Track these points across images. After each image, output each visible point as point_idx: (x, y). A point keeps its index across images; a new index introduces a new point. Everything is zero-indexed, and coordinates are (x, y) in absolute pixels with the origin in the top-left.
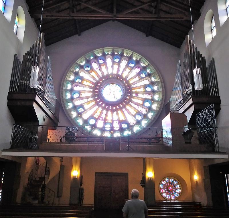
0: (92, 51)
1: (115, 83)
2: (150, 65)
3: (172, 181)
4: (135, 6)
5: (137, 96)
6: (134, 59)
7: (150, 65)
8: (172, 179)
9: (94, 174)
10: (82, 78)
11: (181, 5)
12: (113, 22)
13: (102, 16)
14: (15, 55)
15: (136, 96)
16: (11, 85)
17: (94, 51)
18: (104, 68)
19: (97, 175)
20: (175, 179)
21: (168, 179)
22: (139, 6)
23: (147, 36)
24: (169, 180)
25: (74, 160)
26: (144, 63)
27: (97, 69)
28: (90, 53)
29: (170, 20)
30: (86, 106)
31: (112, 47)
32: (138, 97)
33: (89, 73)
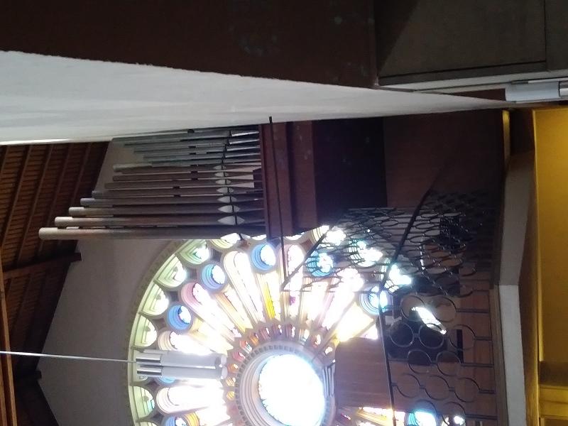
2: (179, 253)
26: (175, 269)
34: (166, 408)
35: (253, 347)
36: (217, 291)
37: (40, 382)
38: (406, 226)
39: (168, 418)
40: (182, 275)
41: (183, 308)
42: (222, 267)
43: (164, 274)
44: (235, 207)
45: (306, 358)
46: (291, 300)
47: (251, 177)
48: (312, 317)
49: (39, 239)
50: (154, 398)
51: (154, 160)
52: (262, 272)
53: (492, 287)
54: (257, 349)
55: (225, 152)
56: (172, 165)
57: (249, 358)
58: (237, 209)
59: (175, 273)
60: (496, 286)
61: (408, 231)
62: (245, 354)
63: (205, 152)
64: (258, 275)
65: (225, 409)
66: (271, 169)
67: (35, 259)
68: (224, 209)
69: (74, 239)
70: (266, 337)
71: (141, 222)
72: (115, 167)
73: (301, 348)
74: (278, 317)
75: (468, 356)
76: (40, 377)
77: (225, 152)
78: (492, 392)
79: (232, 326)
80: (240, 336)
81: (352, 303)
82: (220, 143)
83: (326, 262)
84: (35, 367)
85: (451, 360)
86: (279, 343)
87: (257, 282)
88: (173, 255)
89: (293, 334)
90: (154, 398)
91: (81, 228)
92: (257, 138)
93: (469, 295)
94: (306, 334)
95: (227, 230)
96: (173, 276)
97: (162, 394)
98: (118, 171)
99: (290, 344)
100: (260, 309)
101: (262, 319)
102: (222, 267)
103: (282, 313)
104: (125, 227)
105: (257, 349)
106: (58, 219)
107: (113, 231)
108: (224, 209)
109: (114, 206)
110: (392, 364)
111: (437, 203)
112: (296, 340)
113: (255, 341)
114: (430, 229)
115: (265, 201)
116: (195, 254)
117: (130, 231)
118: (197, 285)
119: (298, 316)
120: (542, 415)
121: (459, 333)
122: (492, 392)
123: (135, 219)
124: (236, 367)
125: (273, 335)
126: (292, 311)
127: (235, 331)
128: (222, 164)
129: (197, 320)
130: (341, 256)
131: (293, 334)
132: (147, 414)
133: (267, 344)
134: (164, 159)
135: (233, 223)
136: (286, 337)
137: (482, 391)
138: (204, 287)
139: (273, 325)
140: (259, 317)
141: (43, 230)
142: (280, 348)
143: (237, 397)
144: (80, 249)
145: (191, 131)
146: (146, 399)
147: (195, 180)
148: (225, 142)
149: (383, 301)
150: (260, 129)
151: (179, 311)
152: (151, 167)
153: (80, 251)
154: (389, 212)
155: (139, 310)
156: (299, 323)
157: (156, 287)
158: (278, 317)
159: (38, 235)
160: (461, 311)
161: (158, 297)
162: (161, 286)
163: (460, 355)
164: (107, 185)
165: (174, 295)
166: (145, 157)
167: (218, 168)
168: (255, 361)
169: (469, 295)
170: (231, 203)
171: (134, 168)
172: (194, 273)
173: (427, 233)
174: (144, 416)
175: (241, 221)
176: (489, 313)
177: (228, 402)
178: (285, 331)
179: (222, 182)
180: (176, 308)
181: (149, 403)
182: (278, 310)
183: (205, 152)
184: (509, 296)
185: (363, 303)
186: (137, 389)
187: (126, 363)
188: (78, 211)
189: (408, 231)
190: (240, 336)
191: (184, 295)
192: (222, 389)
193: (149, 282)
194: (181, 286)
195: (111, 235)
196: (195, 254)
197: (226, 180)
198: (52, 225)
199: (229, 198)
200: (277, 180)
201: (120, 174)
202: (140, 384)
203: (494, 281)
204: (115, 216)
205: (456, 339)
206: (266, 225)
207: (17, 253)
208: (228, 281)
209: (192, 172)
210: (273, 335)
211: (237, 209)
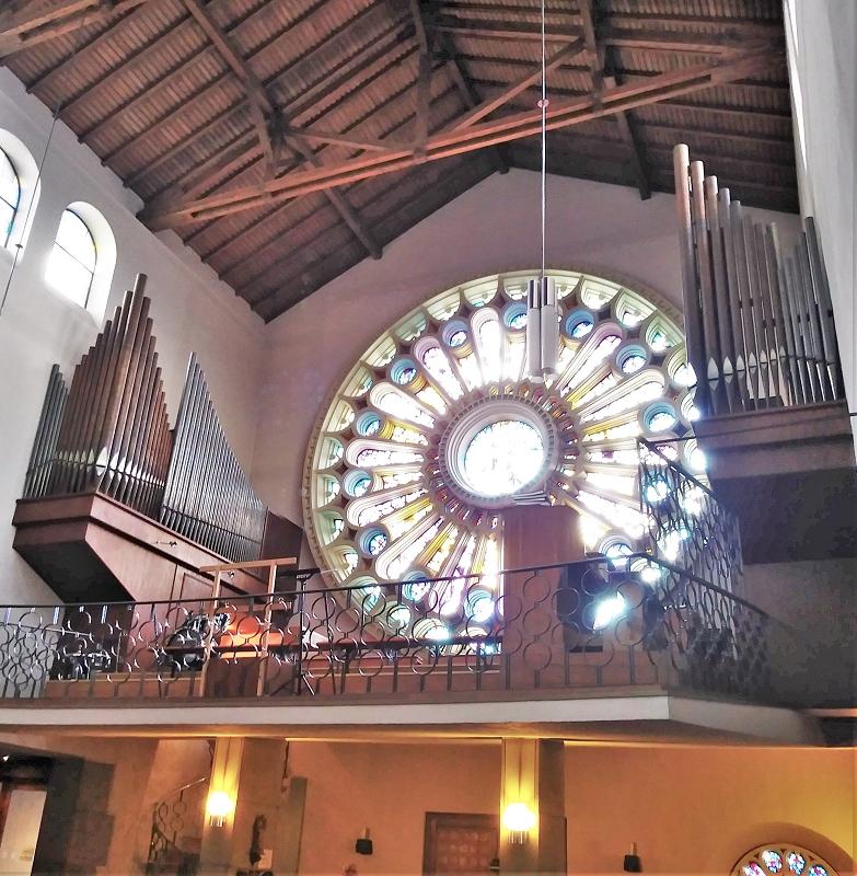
0: (418, 305)
1: (512, 416)
2: (658, 315)
3: (800, 866)
4: (504, 85)
5: (611, 460)
6: (516, 294)
7: (658, 315)
8: (800, 859)
9: (422, 819)
10: (384, 419)
11: (696, 26)
12: (504, 176)
13: (372, 162)
14: (55, 367)
15: (606, 460)
16: (30, 473)
17: (426, 304)
18: (468, 367)
19: (433, 823)
20: (812, 859)
21: (775, 857)
22: (522, 80)
23: (646, 196)
24: (782, 861)
25: (510, 754)
26: (637, 313)
27: (443, 371)
28: (411, 317)
29: (659, 102)
30: (395, 526)
31: (496, 276)
32: (615, 464)
33: (414, 395)
34: (476, 320)
35: (551, 412)
36: (613, 365)
37: (497, 174)
38: (723, 587)
39: (436, 337)
40: (631, 321)
41: (591, 326)
42: (644, 368)
43: (630, 300)
44: (717, 382)
45: (541, 473)
46: (608, 453)
47: (773, 393)
48: (590, 478)
49: (672, 148)
50: (486, 305)
51: (787, 272)
52: (640, 416)
53: (664, 688)
54: (549, 417)
55: (805, 360)
56: (783, 297)
57: (537, 408)
58: (728, 380)
59: (632, 312)
60: (666, 692)
61: (717, 590)
62: (541, 403)
63: (803, 333)
64: (636, 412)
65: (479, 385)
66: (785, 419)
67: (641, 145)
68: (727, 364)
69: (678, 190)
70: (562, 425)
71: (704, 264)
72: (773, 224)
73: (552, 467)
74: (587, 439)
75: (575, 658)
76: (502, 173)
77: (805, 360)
78: (537, 685)
79: (572, 385)
80: (562, 395)
81: (610, 525)
82: (816, 353)
83: (658, 493)
84: (514, 165)
85: (566, 637)
86: (557, 441)
87: (627, 411)
88: (655, 308)
89: (569, 457)
90: (486, 305)
91: (691, 194)
92: (826, 398)
93: (651, 660)
94: (569, 473)
95: (701, 369)
96: (628, 310)
97: (491, 313)
98: (769, 230)
99: (556, 454)
100: (599, 416)
101: (583, 420)
102: (644, 368)
103: (591, 443)
104: (695, 246)
105: (549, 417)
106: (700, 164)
107: (689, 231)
108: (727, 364)
109: (722, 230)
110: (556, 574)
111: (752, 625)
112: (562, 461)
113: (557, 414)
114: (721, 616)
115: (741, 414)
116: (658, 334)
117: (691, 253)
118: (618, 341)
119: (590, 462)
120: (505, 741)
121: (600, 649)
122: (537, 685)
123: (720, 248)
124: (526, 395)
125: (567, 436)
126: (596, 456)
127: (566, 390)
128: (787, 357)
129: (578, 344)
130: (667, 513)
131: (569, 457)
132: (469, 299)
133: (554, 427)
134: (788, 283)
135: (710, 376)
136: (564, 449)
137: (537, 674)
138: (618, 349)
139: (575, 435)
140: (586, 418)
141: (684, 149)
142: (552, 443)
143: (493, 397)
144: (659, 198)
145: (830, 313)
146: (485, 296)
147: (764, 324)
148: (819, 357)
149: (618, 558)
150: (841, 401)
151: (587, 323)
152: (776, 269)
153: (653, 198)
154: (738, 567)
155: (586, 276)
156: (581, 465)
157: (615, 293)
158: (587, 439)
159: (678, 143)
160: (631, 653)
161: (602, 297)
162: (615, 299)
163: (577, 650)
164: (749, 217)
165: (606, 314)
166: (789, 261)
167: (783, 353)
168: (534, 414)
169: (651, 660)
170: (722, 375)
171: (774, 250)
172: (634, 336)
173: (700, 607)
174: (505, 285)
175: (714, 385)
176: (630, 685)
177: (487, 388)
178: (571, 447)
179: (763, 358)
180: (590, 318)
181: (482, 299)
182: (596, 438)
183: (803, 333)
184: (656, 707)
185: (611, 538)
186: (495, 285)
187: (540, 268)
188: (711, 185)
189: (717, 590)
190: (562, 395)
191: (606, 327)
192: (483, 384)
193: (621, 283)
194: (617, 321)
195: (685, 230)
196: (658, 334)
197: (776, 360)
198: (692, 160)
199: (717, 376)
200: (771, 427)
201: (764, 232)
202: (501, 288)
203: (672, 691)
204: (709, 233)
205: (594, 645)
206: (710, 417)
207: (649, 123)
208: (627, 377)
209: (774, 320)
210: (567, 436)
211: (728, 380)
